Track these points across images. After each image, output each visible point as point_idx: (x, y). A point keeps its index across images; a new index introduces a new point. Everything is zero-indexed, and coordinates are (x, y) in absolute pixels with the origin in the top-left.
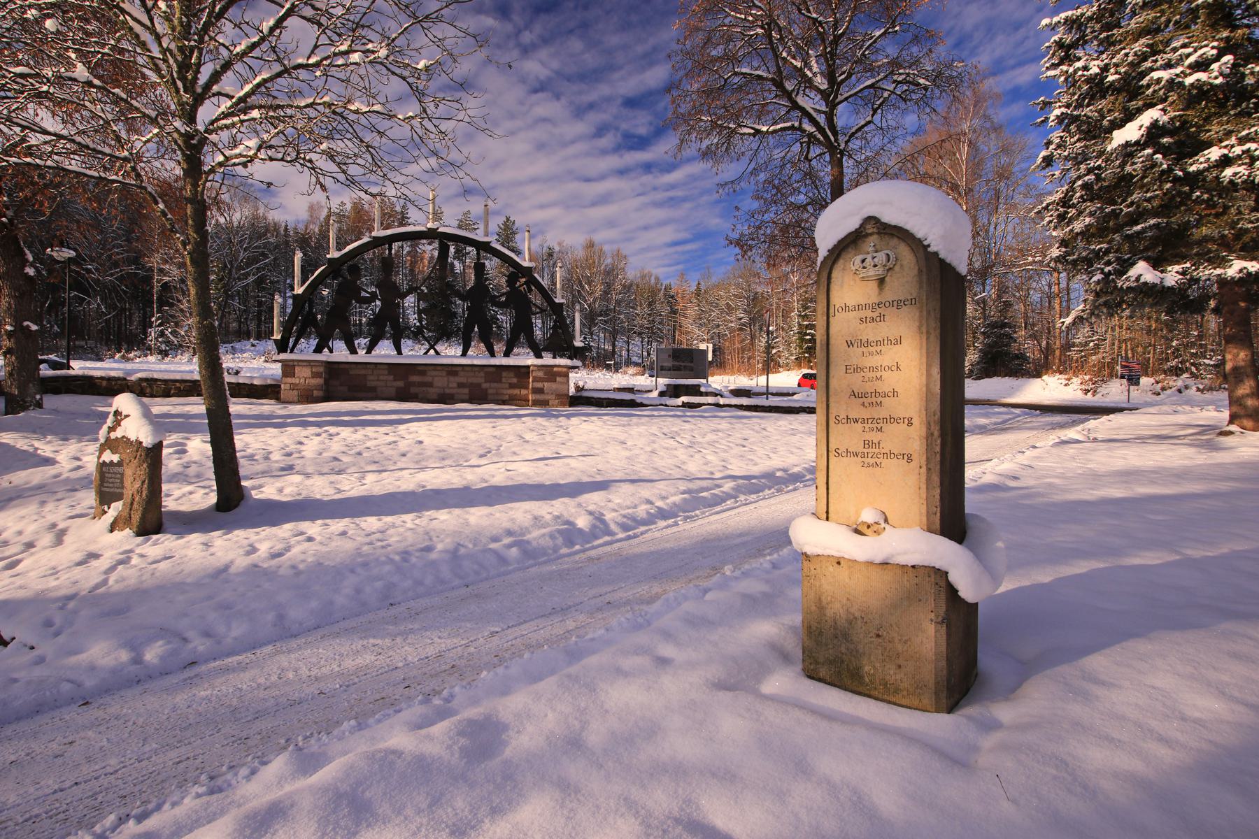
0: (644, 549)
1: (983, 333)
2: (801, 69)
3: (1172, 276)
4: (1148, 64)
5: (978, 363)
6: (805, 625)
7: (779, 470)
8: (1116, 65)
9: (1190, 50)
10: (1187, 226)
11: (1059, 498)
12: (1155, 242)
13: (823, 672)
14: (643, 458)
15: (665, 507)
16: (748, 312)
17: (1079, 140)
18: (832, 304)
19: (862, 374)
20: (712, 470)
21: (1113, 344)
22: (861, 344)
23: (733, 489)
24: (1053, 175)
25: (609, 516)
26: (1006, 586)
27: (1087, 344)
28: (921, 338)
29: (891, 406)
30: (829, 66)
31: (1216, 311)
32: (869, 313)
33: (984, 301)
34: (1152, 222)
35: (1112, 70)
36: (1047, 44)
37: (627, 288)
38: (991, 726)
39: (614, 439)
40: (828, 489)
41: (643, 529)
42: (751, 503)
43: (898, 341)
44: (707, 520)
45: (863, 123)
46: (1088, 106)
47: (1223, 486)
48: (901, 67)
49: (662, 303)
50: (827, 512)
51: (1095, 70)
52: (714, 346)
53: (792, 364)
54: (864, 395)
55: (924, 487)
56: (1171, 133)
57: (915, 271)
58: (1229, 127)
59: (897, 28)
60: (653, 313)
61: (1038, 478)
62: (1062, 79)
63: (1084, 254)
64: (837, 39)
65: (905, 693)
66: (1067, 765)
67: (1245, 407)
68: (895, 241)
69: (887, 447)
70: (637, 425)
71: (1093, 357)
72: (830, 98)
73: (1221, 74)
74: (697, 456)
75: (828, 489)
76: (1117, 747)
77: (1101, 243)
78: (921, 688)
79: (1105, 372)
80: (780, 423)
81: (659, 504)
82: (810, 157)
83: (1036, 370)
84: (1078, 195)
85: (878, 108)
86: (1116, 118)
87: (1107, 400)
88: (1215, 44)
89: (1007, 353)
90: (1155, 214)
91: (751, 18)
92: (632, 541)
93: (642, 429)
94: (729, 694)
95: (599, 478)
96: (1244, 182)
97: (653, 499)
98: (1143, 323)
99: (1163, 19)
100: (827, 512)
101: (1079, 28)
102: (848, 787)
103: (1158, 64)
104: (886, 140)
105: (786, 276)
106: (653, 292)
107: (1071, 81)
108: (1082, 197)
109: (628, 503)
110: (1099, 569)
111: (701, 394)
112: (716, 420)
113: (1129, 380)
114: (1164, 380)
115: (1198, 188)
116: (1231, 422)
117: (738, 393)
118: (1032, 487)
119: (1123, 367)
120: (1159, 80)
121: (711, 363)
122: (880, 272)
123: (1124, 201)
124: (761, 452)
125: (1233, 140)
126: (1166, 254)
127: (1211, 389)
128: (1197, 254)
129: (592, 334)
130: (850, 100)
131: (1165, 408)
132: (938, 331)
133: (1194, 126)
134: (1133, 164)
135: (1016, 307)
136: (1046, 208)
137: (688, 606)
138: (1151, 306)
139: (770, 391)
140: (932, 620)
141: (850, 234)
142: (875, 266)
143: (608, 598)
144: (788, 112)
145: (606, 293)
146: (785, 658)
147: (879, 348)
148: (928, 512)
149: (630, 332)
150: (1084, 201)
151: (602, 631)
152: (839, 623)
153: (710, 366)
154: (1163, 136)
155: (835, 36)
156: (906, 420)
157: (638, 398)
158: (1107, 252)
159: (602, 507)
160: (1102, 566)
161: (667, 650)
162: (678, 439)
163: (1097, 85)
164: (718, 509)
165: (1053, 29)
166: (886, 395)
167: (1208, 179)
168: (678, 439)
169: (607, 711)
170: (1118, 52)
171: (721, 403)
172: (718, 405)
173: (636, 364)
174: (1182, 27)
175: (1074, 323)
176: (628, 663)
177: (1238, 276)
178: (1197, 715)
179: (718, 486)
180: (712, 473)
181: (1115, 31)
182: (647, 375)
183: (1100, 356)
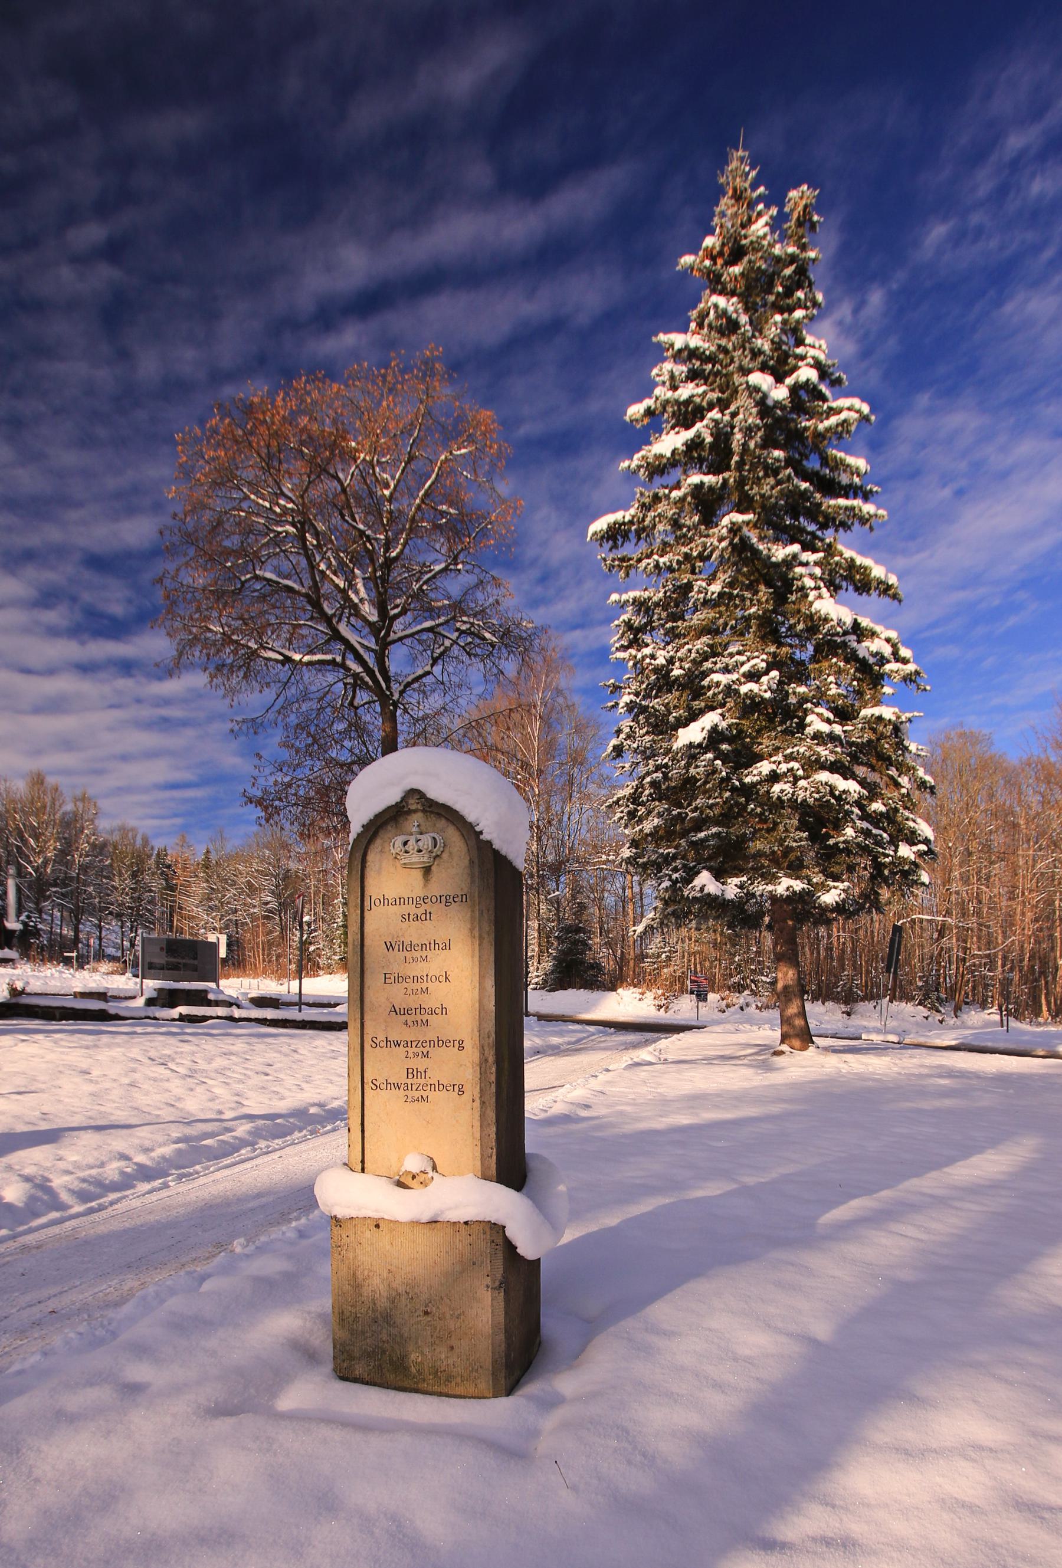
0: (115, 1226)
1: (557, 938)
2: (343, 592)
3: (731, 888)
4: (708, 665)
5: (552, 972)
6: (336, 1311)
7: (314, 1105)
8: (681, 660)
9: (743, 658)
10: (743, 840)
11: (630, 1128)
12: (719, 851)
13: (359, 1370)
14: (116, 1094)
15: (149, 1163)
16: (277, 895)
17: (647, 733)
18: (367, 894)
19: (405, 985)
20: (220, 1107)
21: (683, 957)
22: (403, 947)
23: (250, 1133)
24: (623, 767)
25: (58, 1182)
26: (568, 1236)
27: (659, 956)
28: (473, 944)
29: (438, 1026)
30: (379, 593)
31: (770, 927)
32: (412, 909)
33: (557, 900)
34: (714, 830)
35: (677, 664)
36: (616, 622)
37: (99, 849)
38: (550, 1403)
39: (71, 1067)
40: (363, 1131)
41: (113, 1196)
42: (275, 1150)
43: (447, 946)
44: (212, 1177)
45: (420, 672)
46: (656, 697)
47: (775, 1109)
48: (464, 613)
49: (153, 874)
50: (363, 1162)
51: (661, 661)
52: (229, 937)
53: (335, 967)
54: (407, 1011)
55: (477, 1124)
56: (730, 740)
57: (467, 862)
58: (777, 743)
59: (460, 567)
60: (139, 888)
61: (609, 1106)
62: (631, 663)
63: (653, 857)
64: (389, 563)
65: (459, 1380)
66: (628, 1433)
67: (794, 1027)
68: (442, 823)
69: (434, 1077)
70: (109, 1046)
71: (665, 970)
72: (381, 630)
73: (770, 688)
74: (200, 1089)
75: (363, 1131)
76: (676, 1402)
77: (669, 847)
78: (477, 1371)
79: (676, 987)
80: (317, 1043)
81: (141, 1158)
82: (356, 703)
83: (611, 981)
84: (647, 792)
85: (438, 658)
86: (680, 716)
87: (679, 1017)
88: (764, 657)
89: (582, 962)
90: (717, 824)
91: (278, 510)
92: (95, 1216)
93: (116, 1052)
94: (230, 1421)
95: (44, 1126)
96: (789, 800)
97: (130, 1152)
98: (706, 936)
99: (721, 621)
100: (363, 1162)
101: (647, 612)
102: (385, 1515)
103: (719, 666)
104: (448, 699)
105: (326, 852)
106: (140, 859)
107: (639, 666)
108: (650, 795)
109: (91, 1160)
110: (664, 1206)
111: (209, 1003)
112: (229, 1040)
113: (697, 996)
114: (729, 996)
115: (753, 800)
116: (782, 1042)
117: (261, 1002)
118: (604, 1117)
119: (692, 981)
120: (718, 684)
121: (224, 961)
122: (426, 859)
123: (689, 805)
124: (290, 1082)
125: (779, 757)
126: (726, 866)
127: (767, 1007)
128: (752, 868)
129: (40, 911)
130: (406, 641)
131: (729, 1026)
132: (493, 936)
133: (749, 736)
134: (697, 767)
135: (591, 910)
136: (617, 802)
137: (174, 1303)
138: (715, 918)
139: (304, 1000)
140: (488, 1287)
141: (389, 809)
142: (420, 851)
143: (52, 1305)
144: (328, 642)
145: (63, 854)
146: (311, 1357)
147: (424, 954)
148: (482, 1155)
149: (100, 912)
150: (653, 800)
151: (37, 1357)
152: (378, 1304)
153: (223, 966)
154: (722, 742)
155: (386, 558)
156: (456, 1043)
157: (112, 1007)
158: (675, 857)
159: (47, 1169)
160: (672, 1200)
161: (139, 1372)
162: (171, 1065)
163: (664, 677)
164: (228, 1161)
165: (622, 607)
166: (433, 1012)
167: (760, 793)
168: (171, 1065)
169: (37, 1480)
170: (683, 646)
171: (236, 1016)
172: (231, 1019)
173: (113, 959)
174: (739, 633)
175: (645, 932)
176: (73, 1402)
177: (786, 894)
178: (747, 1352)
179: (229, 1130)
180: (220, 1112)
181: (679, 623)
182: (129, 975)
183: (672, 969)
